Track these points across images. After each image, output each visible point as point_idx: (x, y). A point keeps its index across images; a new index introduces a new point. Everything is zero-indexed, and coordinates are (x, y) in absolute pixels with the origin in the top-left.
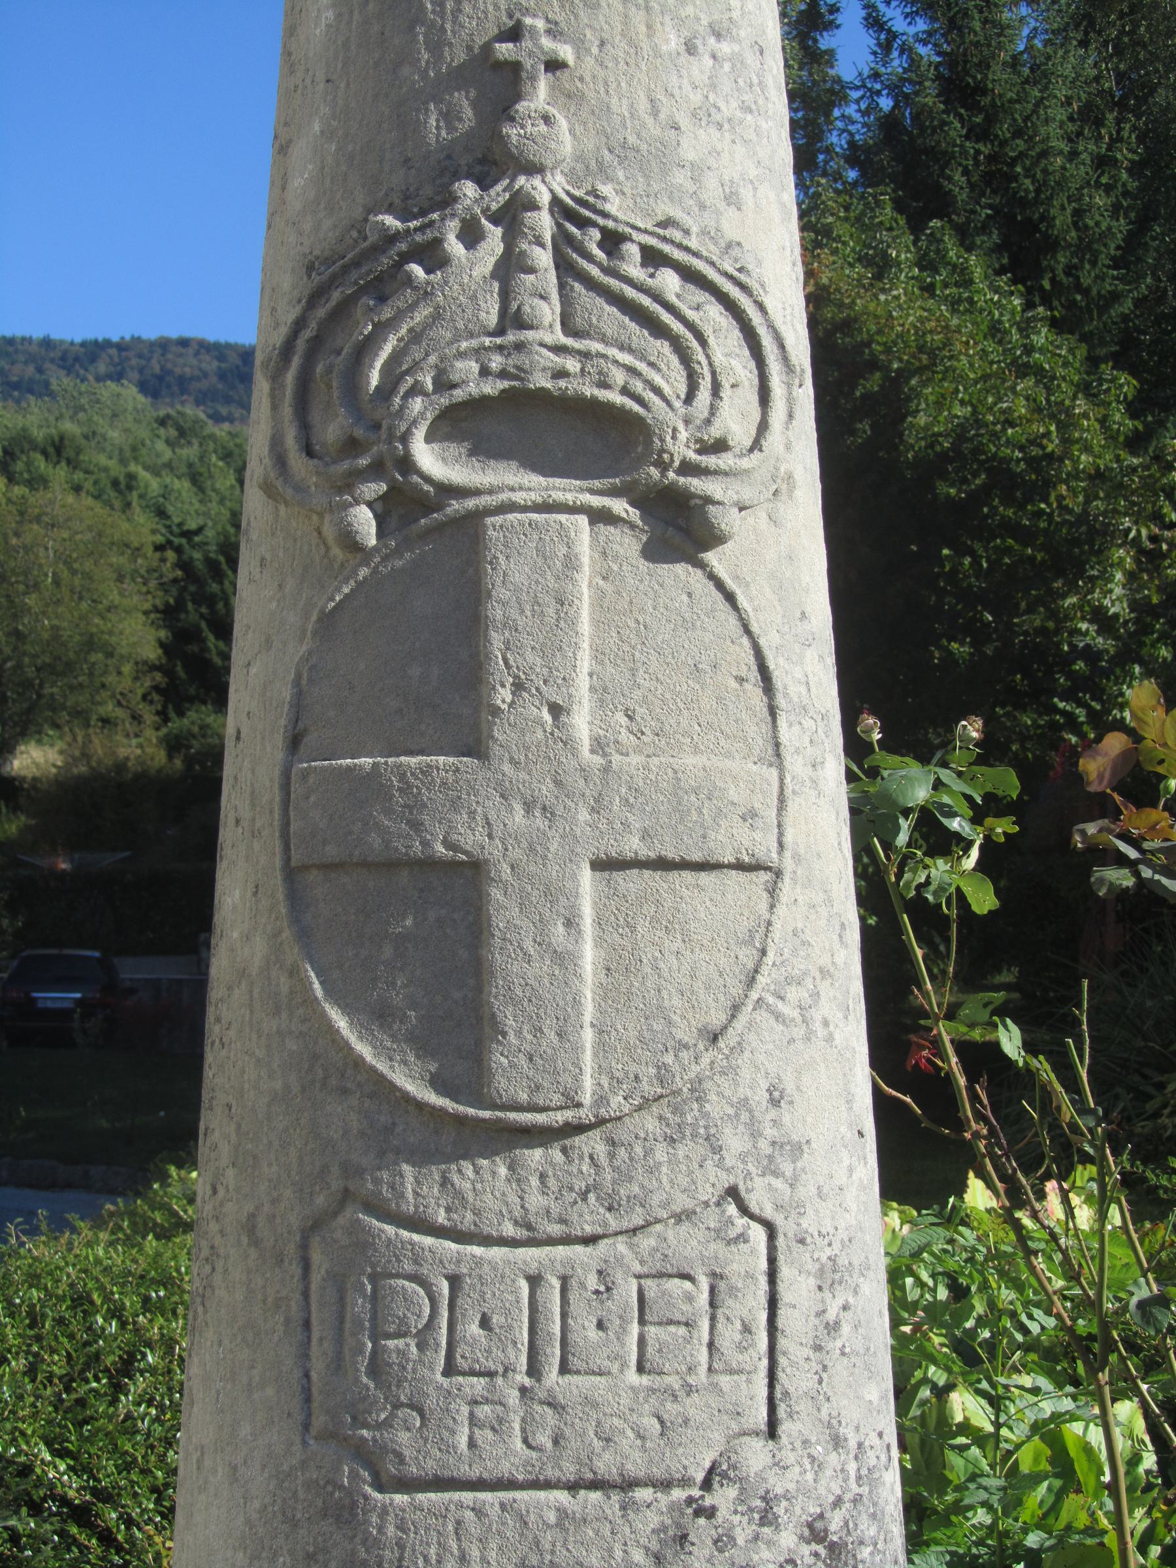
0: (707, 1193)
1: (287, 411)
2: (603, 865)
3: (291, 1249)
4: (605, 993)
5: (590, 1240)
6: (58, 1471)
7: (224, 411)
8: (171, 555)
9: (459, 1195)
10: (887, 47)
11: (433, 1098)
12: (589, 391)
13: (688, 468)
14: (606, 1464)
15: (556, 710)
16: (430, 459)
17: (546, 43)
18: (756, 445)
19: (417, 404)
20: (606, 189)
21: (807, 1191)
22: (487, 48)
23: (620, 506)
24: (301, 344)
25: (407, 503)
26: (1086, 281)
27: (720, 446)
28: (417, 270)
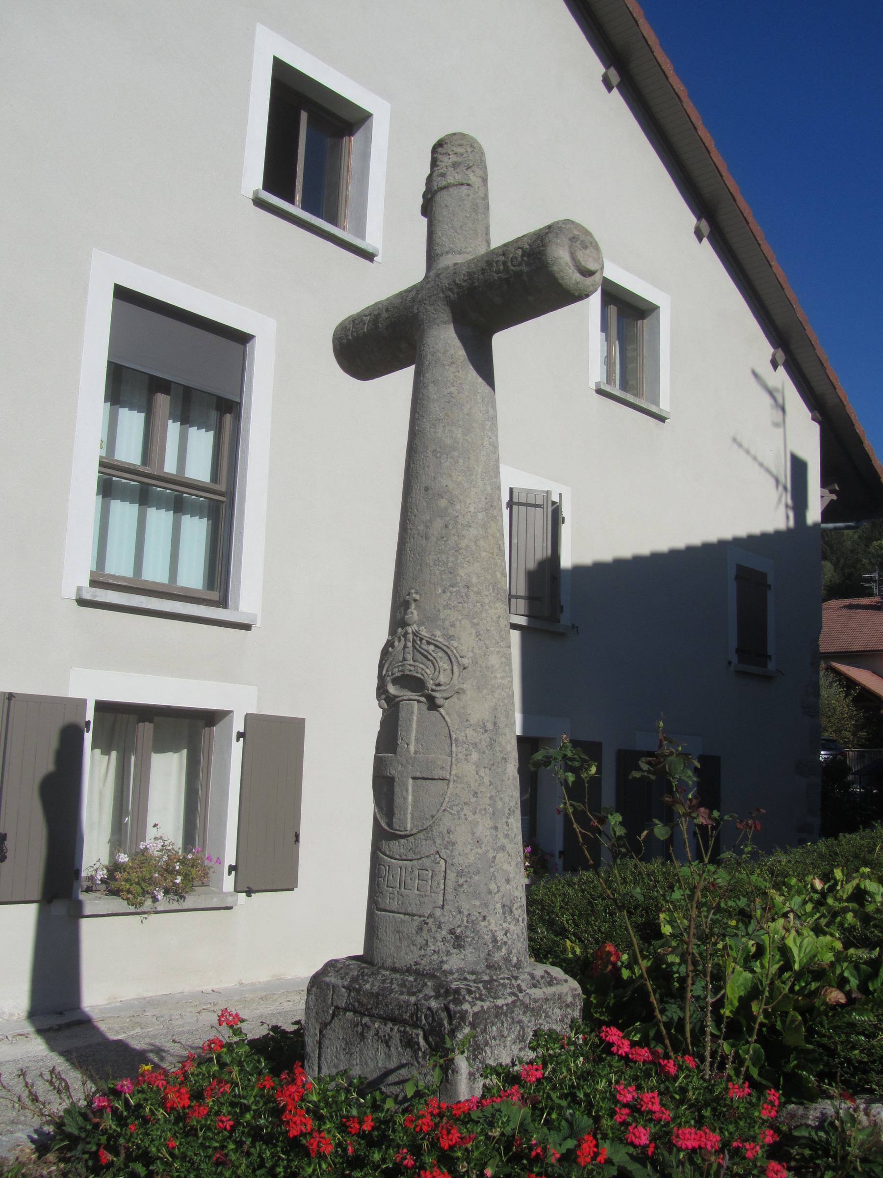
2: (414, 778)
4: (413, 806)
5: (411, 860)
12: (415, 674)
13: (433, 690)
14: (409, 910)
17: (414, 595)
21: (456, 853)
23: (423, 699)
27: (439, 685)
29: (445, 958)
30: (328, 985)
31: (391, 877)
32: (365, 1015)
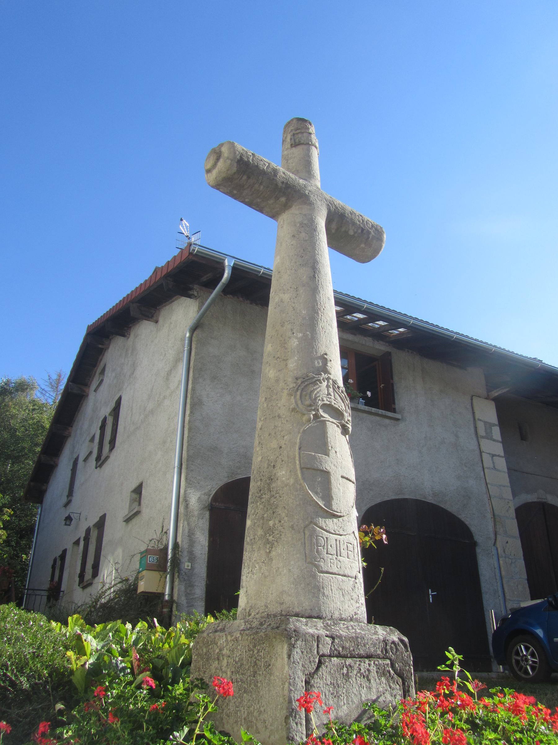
3: (302, 530)
5: (341, 535)
11: (324, 507)
31: (329, 547)
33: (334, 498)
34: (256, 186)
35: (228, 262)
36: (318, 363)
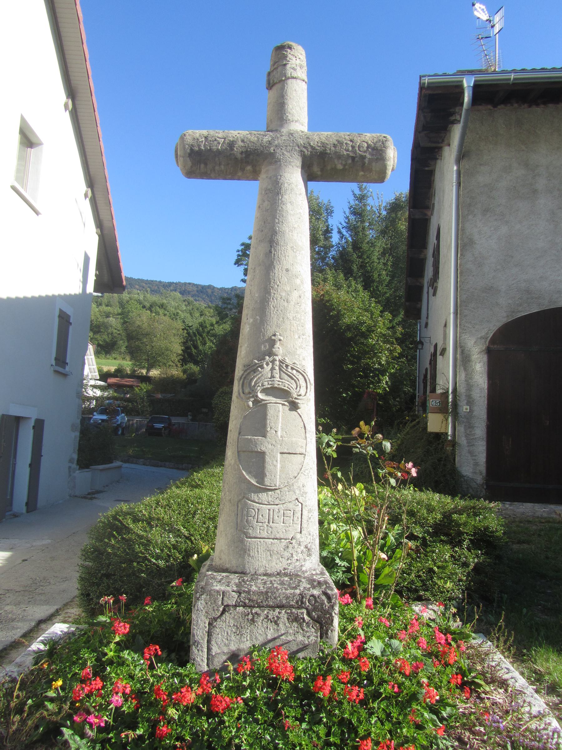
0: (294, 499)
1: (240, 387)
2: (281, 453)
4: (281, 471)
5: (277, 505)
6: (184, 530)
7: (197, 299)
8: (186, 331)
9: (259, 498)
10: (342, 238)
12: (283, 387)
13: (296, 398)
14: (278, 536)
15: (276, 431)
16: (261, 396)
17: (279, 337)
18: (305, 395)
19: (259, 388)
20: (286, 358)
21: (307, 499)
22: (271, 337)
23: (286, 403)
24: (243, 378)
25: (257, 402)
26: (380, 289)
27: (300, 395)
28: (260, 369)
29: (303, 563)
30: (218, 592)
32: (254, 607)
33: (268, 474)
34: (217, 168)
35: (467, 82)
36: (265, 347)
